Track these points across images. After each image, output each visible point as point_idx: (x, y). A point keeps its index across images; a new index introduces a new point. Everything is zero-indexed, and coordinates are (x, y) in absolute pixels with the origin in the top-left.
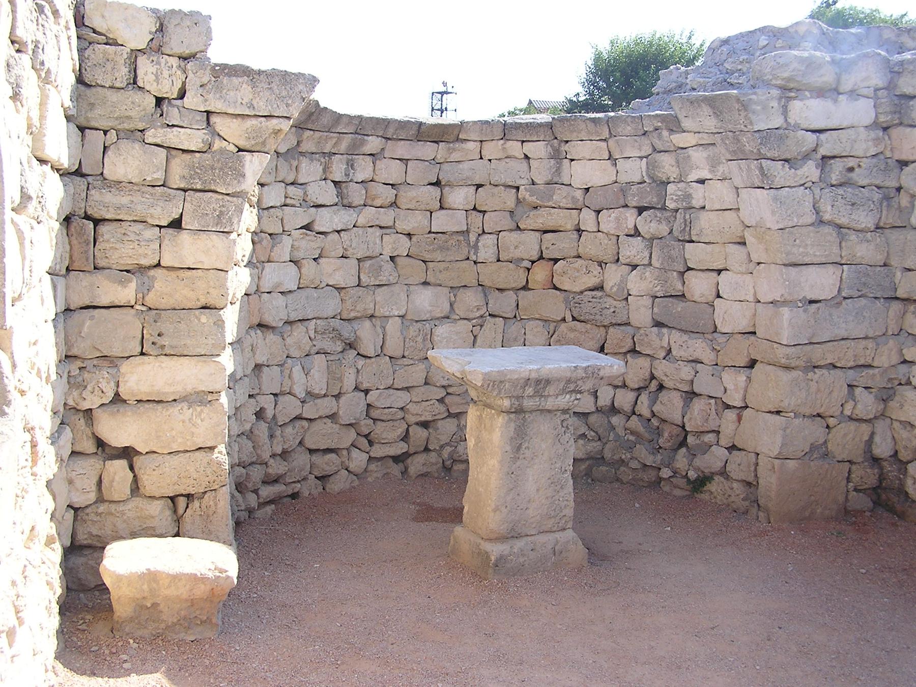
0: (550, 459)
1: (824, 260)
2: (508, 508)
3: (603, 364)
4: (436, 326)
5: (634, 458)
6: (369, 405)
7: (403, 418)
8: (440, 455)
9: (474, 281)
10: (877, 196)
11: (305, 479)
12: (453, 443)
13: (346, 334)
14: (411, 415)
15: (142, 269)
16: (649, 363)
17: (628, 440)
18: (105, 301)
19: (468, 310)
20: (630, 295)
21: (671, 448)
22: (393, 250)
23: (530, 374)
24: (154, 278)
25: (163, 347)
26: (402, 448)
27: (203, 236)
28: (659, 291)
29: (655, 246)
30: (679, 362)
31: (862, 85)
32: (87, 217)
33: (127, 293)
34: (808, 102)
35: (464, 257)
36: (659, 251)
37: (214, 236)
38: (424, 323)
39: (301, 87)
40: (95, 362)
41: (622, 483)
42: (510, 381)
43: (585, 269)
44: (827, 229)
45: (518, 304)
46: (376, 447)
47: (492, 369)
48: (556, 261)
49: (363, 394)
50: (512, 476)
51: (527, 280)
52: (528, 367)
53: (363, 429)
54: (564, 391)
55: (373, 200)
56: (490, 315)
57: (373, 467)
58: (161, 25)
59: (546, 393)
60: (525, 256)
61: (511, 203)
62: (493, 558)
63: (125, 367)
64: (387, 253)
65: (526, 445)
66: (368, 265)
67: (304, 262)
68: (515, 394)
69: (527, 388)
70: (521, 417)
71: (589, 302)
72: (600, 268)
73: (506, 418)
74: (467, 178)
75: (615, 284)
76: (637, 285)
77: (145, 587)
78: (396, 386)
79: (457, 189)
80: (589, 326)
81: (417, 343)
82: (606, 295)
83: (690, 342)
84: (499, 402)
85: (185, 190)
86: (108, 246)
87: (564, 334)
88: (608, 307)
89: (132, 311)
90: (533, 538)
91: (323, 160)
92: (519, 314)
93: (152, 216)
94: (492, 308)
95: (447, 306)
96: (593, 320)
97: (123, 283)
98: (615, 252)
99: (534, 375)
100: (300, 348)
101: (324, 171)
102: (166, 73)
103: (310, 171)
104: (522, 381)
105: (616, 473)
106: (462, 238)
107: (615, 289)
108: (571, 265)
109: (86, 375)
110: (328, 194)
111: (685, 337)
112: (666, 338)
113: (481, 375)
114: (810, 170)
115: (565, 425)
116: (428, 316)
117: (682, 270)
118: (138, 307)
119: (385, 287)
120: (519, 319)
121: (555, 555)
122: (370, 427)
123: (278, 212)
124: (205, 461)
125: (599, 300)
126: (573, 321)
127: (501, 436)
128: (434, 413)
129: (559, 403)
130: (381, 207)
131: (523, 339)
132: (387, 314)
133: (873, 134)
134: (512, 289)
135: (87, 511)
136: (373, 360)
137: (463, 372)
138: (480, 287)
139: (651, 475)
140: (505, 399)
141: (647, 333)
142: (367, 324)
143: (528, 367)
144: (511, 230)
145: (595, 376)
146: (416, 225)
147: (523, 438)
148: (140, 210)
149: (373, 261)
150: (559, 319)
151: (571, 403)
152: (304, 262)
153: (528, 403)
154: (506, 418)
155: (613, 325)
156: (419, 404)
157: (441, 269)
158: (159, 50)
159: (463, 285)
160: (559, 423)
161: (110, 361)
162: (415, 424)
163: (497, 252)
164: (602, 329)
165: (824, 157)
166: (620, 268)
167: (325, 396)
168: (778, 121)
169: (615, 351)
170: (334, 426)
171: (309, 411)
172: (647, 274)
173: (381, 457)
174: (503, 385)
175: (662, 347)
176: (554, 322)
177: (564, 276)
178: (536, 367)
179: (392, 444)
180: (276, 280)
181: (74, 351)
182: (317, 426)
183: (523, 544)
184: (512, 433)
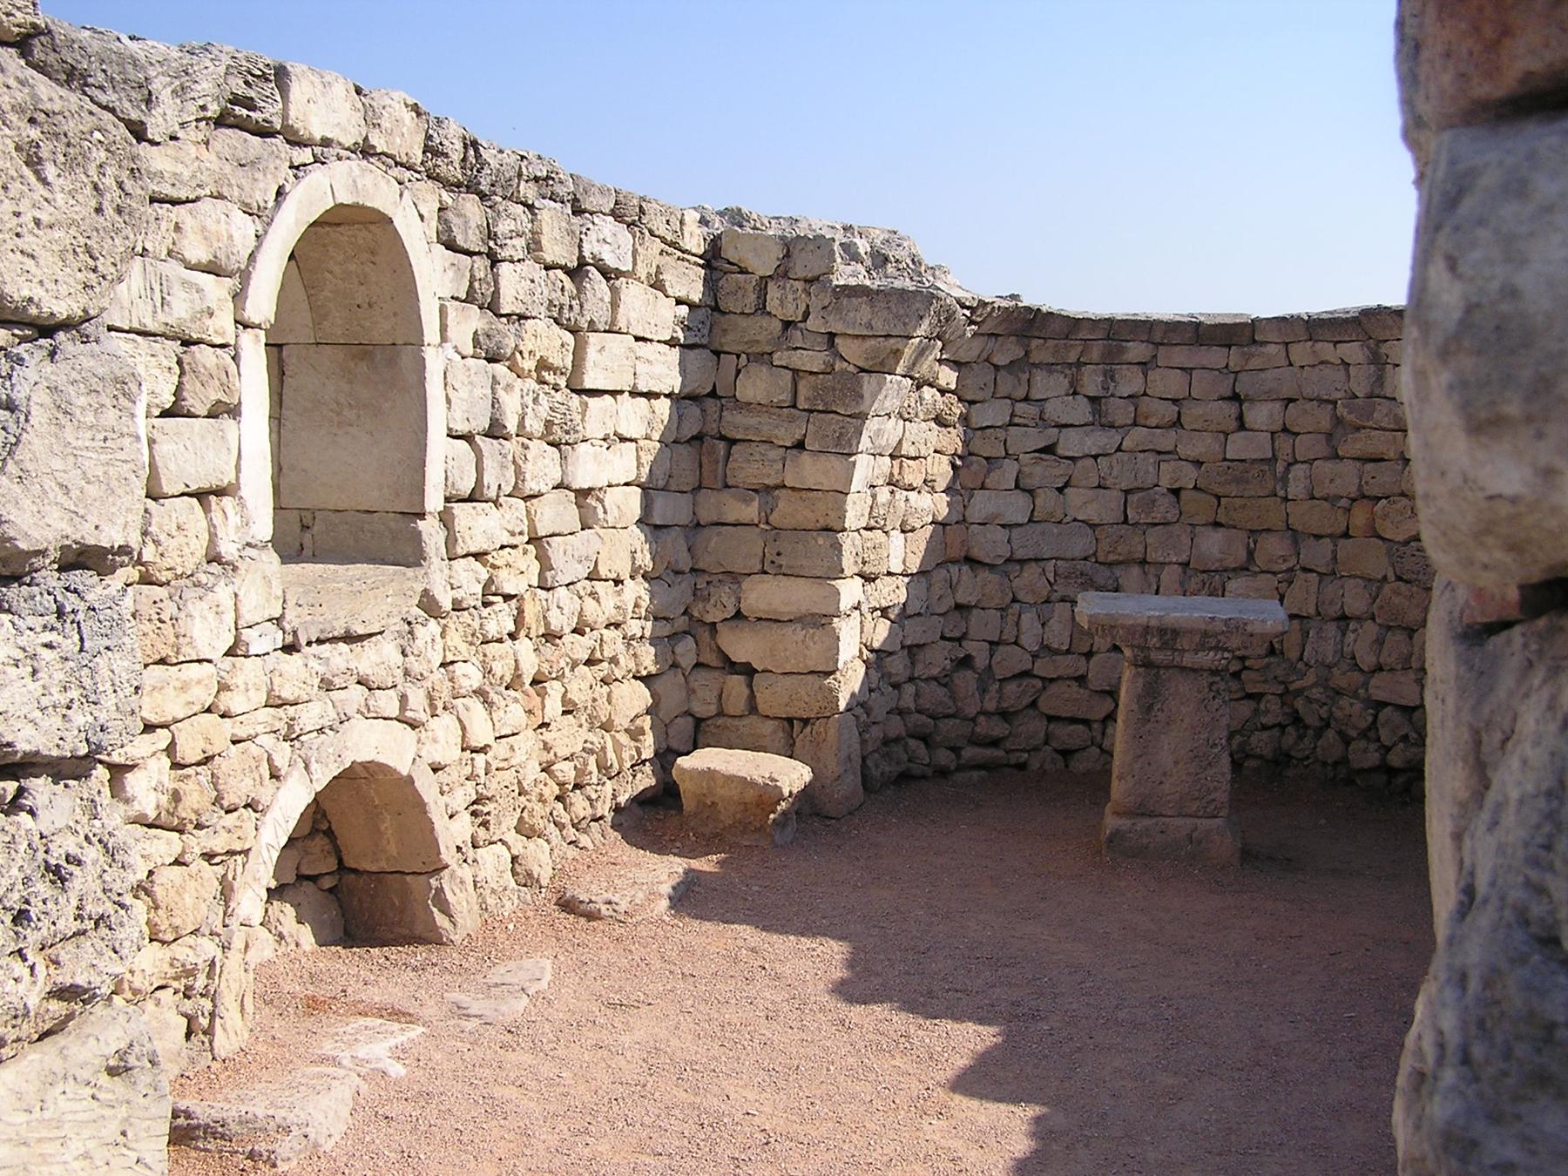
0: (1193, 728)
11: (1036, 749)
15: (768, 489)
18: (731, 519)
19: (1270, 561)
24: (778, 498)
25: (781, 566)
27: (823, 457)
32: (722, 438)
33: (750, 512)
37: (832, 458)
39: (918, 305)
40: (720, 577)
42: (1123, 626)
51: (627, 484)
54: (1201, 647)
55: (1146, 418)
58: (788, 251)
61: (1326, 424)
63: (746, 584)
64: (1165, 482)
67: (1038, 491)
74: (1270, 391)
77: (704, 784)
79: (1258, 404)
85: (812, 411)
86: (736, 465)
89: (757, 530)
91: (1067, 371)
93: (777, 437)
97: (747, 502)
100: (1033, 592)
101: (1071, 384)
102: (790, 297)
103: (1048, 385)
106: (1267, 468)
109: (712, 589)
110: (1080, 411)
118: (762, 526)
123: (1001, 434)
124: (816, 686)
130: (1157, 427)
134: (1330, 536)
135: (709, 722)
146: (1203, 450)
148: (766, 431)
152: (1038, 491)
158: (785, 275)
161: (735, 577)
167: (1068, 652)
170: (1082, 691)
171: (1043, 668)
181: (701, 565)
182: (1054, 689)
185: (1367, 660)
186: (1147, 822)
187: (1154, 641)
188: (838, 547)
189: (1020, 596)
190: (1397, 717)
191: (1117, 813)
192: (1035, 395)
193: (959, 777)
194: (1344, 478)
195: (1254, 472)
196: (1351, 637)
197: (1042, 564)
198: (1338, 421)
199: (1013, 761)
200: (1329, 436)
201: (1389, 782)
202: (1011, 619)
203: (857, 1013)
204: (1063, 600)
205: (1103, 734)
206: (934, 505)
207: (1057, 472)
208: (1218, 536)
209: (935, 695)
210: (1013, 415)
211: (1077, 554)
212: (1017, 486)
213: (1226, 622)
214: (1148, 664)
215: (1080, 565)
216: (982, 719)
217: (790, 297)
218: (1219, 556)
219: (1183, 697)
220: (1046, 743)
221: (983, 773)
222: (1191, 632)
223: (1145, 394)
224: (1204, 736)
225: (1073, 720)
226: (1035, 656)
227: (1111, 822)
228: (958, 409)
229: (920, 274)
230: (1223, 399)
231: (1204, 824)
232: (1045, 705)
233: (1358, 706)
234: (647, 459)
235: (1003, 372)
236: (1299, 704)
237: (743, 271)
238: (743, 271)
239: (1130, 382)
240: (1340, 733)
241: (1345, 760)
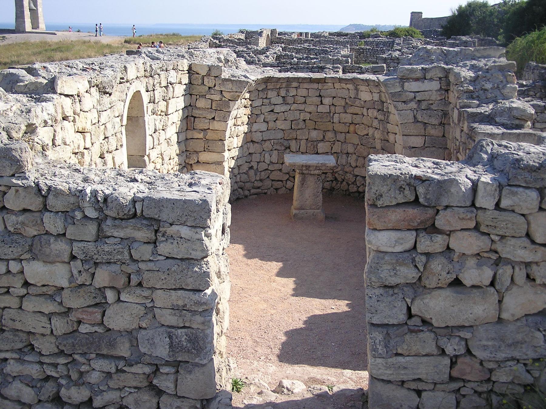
1: (417, 134)
10: (440, 114)
11: (269, 189)
13: (285, 144)
27: (220, 122)
31: (434, 76)
32: (192, 116)
33: (201, 136)
34: (411, 83)
37: (222, 122)
44: (419, 124)
54: (316, 169)
61: (343, 104)
63: (200, 154)
64: (302, 118)
85: (216, 110)
95: (322, 137)
97: (200, 133)
100: (268, 148)
101: (278, 93)
102: (211, 81)
103: (272, 94)
109: (191, 155)
110: (280, 100)
114: (413, 105)
123: (260, 108)
133: (439, 93)
144: (343, 113)
148: (204, 115)
153: (305, 172)
161: (197, 152)
165: (418, 100)
167: (277, 163)
168: (399, 89)
171: (270, 168)
180: (258, 128)
182: (273, 173)
185: (353, 164)
186: (303, 211)
187: (304, 168)
188: (224, 145)
189: (265, 149)
190: (361, 179)
191: (295, 209)
192: (268, 97)
193: (250, 197)
194: (348, 118)
195: (325, 115)
196: (349, 158)
197: (270, 141)
198: (347, 103)
199: (263, 192)
200: (344, 107)
201: (359, 195)
202: (263, 156)
203: (249, 261)
204: (275, 150)
205: (286, 184)
206: (245, 128)
207: (274, 117)
209: (244, 177)
210: (263, 103)
211: (279, 138)
212: (264, 121)
213: (321, 164)
214: (303, 174)
215: (280, 141)
216: (256, 182)
217: (211, 81)
219: (311, 181)
220: (272, 187)
221: (256, 196)
222: (313, 166)
223: (297, 95)
224: (316, 190)
225: (278, 181)
226: (269, 165)
227: (294, 212)
228: (250, 103)
229: (237, 64)
230: (317, 96)
231: (316, 211)
232: (272, 177)
233: (351, 176)
234: (178, 126)
235: (260, 92)
236: (336, 175)
237: (198, 74)
238: (198, 74)
239: (293, 92)
240: (347, 183)
241: (348, 190)
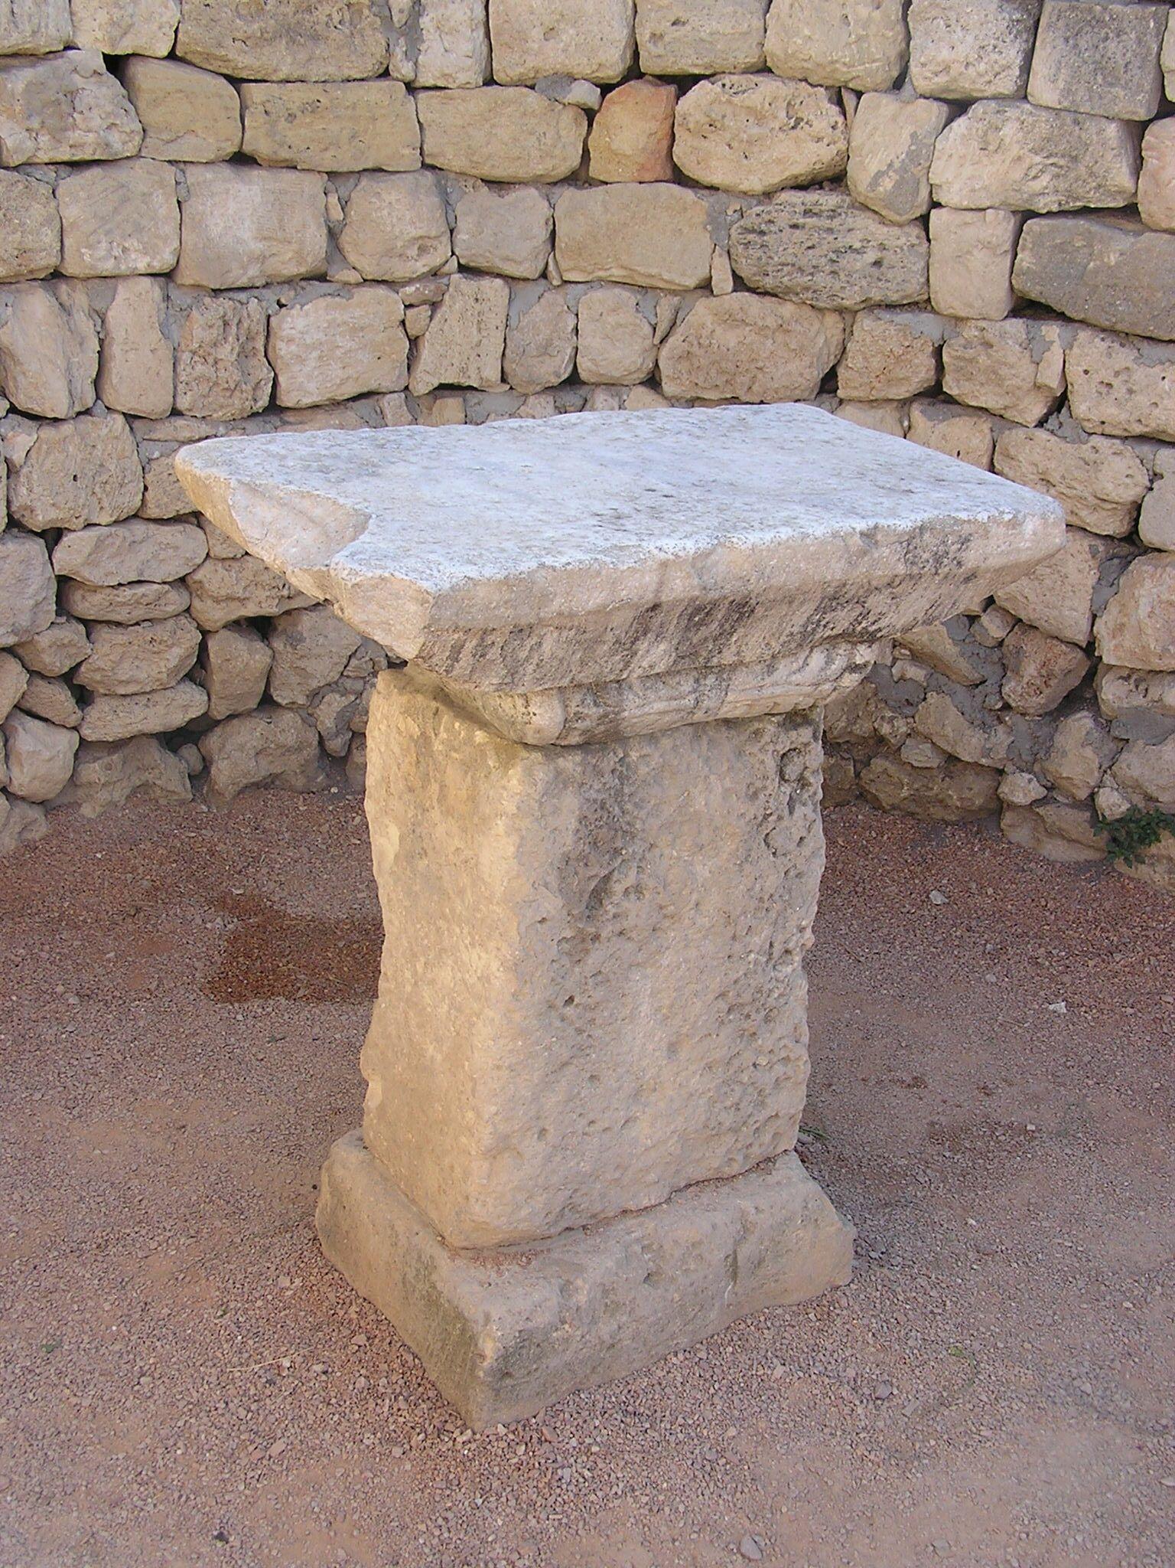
2: (549, 1137)
3: (983, 517)
4: (281, 306)
5: (918, 733)
6: (64, 583)
7: (188, 610)
8: (309, 719)
9: (406, 151)
12: (348, 684)
14: (209, 602)
16: (989, 437)
17: (902, 678)
19: (389, 253)
20: (937, 205)
21: (1041, 712)
22: (116, 33)
23: (661, 583)
26: (186, 708)
28: (1045, 193)
29: (1049, 26)
30: (1095, 440)
35: (370, 66)
36: (1060, 42)
38: (242, 296)
41: (876, 805)
42: (563, 622)
43: (783, 114)
45: (553, 233)
46: (100, 710)
47: (472, 572)
48: (683, 83)
49: (38, 546)
50: (569, 1011)
51: (586, 152)
52: (650, 545)
53: (47, 659)
54: (805, 640)
56: (463, 269)
57: (93, 771)
59: (728, 657)
60: (581, 65)
62: (490, 1348)
65: (631, 879)
66: (20, 87)
68: (585, 677)
69: (642, 646)
70: (610, 761)
71: (795, 226)
72: (835, 109)
73: (542, 774)
75: (890, 165)
76: (968, 171)
78: (153, 512)
80: (787, 309)
81: (220, 365)
82: (852, 206)
83: (1140, 374)
84: (510, 706)
87: (704, 333)
88: (857, 245)
90: (650, 1224)
92: (556, 263)
94: (471, 245)
95: (316, 242)
96: (807, 289)
98: (893, 52)
99: (680, 587)
104: (622, 620)
105: (857, 775)
107: (887, 184)
108: (736, 99)
111: (1124, 356)
112: (1055, 356)
113: (413, 608)
115: (792, 771)
116: (253, 274)
117: (1142, 115)
119: (96, 172)
120: (556, 283)
121: (734, 1276)
122: (74, 651)
125: (827, 223)
126: (734, 291)
127: (519, 855)
128: (285, 593)
129: (778, 690)
131: (569, 351)
132: (108, 267)
134: (536, 181)
136: (67, 428)
137: (323, 579)
138: (428, 173)
139: (973, 791)
140: (535, 700)
141: (989, 336)
142: (39, 303)
143: (650, 545)
145: (943, 571)
147: (617, 852)
149: (42, 69)
150: (691, 282)
151: (827, 687)
154: (542, 774)
155: (873, 307)
156: (236, 565)
157: (295, 110)
159: (370, 165)
160: (771, 764)
162: (224, 627)
163: (485, 49)
164: (831, 319)
166: (910, 108)
169: (875, 395)
172: (1009, 131)
173: (121, 740)
174: (534, 640)
175: (1037, 387)
176: (674, 293)
177: (712, 136)
178: (690, 545)
179: (156, 697)
183: (610, 1264)
184: (569, 839)
208: (251, 188)
213: (910, 541)
218: (257, 247)
